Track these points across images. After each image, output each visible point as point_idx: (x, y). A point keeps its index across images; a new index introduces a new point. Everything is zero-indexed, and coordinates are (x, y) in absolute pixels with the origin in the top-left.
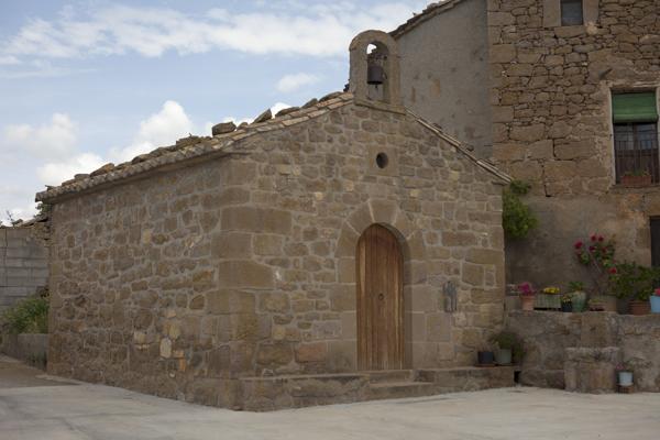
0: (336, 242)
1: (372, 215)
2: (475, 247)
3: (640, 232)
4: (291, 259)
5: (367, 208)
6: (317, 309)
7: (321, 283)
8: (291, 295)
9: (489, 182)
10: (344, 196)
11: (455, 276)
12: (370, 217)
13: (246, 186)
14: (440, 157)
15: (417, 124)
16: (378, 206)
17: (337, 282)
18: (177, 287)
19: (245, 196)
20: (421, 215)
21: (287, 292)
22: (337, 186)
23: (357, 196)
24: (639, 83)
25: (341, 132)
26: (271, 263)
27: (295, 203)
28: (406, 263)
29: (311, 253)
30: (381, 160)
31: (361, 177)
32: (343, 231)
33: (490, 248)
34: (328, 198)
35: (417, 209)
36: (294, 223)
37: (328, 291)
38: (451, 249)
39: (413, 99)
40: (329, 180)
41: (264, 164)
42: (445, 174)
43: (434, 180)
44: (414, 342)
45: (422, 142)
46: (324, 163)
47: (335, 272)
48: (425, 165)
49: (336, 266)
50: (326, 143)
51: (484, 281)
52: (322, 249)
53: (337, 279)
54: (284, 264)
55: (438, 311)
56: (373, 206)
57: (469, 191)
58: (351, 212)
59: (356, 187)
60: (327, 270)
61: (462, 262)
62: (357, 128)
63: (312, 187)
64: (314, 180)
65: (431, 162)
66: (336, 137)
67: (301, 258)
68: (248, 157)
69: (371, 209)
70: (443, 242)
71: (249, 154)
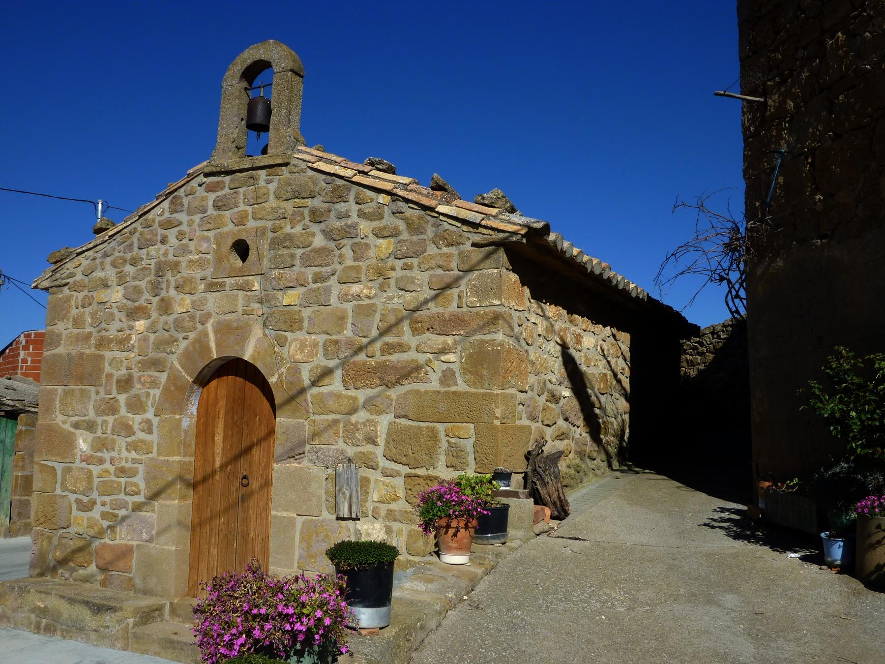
1: (213, 345)
2: (422, 387)
3: (416, 361)
4: (99, 420)
6: (126, 494)
7: (133, 454)
8: (95, 470)
9: (468, 246)
10: (176, 320)
11: (369, 448)
13: (60, 327)
14: (354, 218)
15: (310, 173)
16: (223, 329)
17: (154, 455)
18: (609, 362)
19: (56, 340)
20: (300, 335)
21: (90, 467)
22: (166, 307)
23: (192, 317)
24: (421, 586)
25: (180, 224)
26: (76, 426)
27: (110, 341)
29: (123, 411)
30: (242, 249)
31: (202, 287)
32: (169, 376)
33: (461, 386)
34: (152, 329)
36: (107, 369)
38: (362, 395)
39: (614, 336)
40: (155, 300)
41: (81, 295)
42: (359, 251)
45: (317, 203)
46: (152, 277)
47: (153, 438)
48: (319, 241)
49: (155, 430)
50: (159, 245)
51: (442, 459)
52: (136, 406)
54: (90, 427)
56: (216, 332)
57: (415, 273)
58: (183, 344)
59: (193, 302)
61: (384, 422)
62: (204, 211)
63: (134, 314)
64: (137, 304)
65: (328, 235)
66: (172, 234)
67: (110, 419)
68: (66, 288)
69: (212, 336)
70: (145, 411)
71: (67, 284)
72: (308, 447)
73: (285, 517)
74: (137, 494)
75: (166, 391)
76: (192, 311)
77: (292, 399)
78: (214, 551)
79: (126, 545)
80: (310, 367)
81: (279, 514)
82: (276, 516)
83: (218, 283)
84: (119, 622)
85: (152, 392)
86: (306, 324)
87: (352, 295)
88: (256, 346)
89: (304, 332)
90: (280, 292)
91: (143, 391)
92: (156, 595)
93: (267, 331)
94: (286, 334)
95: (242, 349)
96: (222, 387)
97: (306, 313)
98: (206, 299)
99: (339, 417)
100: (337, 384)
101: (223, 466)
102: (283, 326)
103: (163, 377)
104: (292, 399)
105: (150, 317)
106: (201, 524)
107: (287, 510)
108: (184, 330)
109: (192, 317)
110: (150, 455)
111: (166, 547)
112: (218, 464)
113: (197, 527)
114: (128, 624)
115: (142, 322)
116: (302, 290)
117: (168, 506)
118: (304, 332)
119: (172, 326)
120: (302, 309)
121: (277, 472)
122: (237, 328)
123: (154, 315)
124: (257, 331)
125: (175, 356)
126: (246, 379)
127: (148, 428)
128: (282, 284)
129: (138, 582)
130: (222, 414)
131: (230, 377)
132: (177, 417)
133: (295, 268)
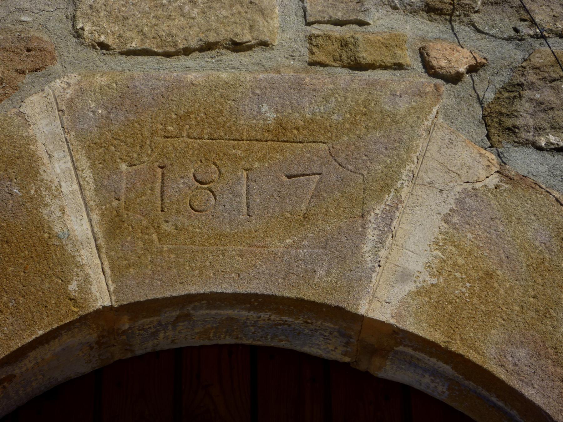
12: (44, 251)
93: (524, 161)
122: (281, 133)
124: (448, 160)
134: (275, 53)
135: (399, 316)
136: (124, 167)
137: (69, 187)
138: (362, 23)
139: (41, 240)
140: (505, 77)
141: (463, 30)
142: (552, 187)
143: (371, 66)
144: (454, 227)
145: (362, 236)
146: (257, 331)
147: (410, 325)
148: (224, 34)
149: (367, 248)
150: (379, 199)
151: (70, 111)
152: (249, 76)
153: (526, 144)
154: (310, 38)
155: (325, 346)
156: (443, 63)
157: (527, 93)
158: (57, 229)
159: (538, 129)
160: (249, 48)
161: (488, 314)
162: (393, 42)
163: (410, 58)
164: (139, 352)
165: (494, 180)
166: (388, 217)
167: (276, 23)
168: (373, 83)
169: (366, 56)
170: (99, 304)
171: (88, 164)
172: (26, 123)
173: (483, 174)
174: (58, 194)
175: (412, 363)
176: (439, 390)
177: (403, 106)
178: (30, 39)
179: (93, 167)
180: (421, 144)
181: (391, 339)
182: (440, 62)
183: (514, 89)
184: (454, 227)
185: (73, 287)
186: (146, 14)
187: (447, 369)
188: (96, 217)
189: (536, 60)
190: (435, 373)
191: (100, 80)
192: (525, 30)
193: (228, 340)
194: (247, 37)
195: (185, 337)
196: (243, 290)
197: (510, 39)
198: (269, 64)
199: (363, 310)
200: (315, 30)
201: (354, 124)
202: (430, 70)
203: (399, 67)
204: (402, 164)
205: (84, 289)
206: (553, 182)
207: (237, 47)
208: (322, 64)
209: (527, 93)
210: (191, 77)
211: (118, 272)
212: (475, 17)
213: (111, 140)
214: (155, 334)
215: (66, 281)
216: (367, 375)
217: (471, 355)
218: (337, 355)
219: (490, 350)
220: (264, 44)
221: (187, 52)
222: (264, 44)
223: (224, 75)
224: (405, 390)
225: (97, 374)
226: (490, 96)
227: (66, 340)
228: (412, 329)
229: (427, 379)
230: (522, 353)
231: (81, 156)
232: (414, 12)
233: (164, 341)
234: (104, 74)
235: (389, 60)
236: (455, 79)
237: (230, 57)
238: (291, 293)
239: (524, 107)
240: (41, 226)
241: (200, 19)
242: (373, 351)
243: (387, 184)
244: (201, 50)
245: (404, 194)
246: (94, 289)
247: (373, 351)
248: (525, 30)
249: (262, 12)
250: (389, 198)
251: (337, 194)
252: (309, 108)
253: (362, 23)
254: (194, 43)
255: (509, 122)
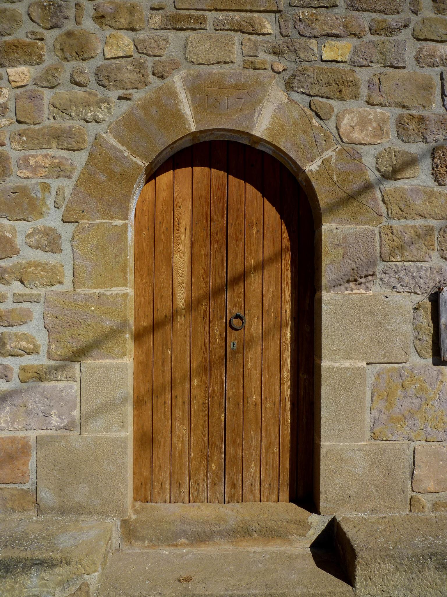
0: (67, 185)
5: (173, 94)
12: (180, 117)
16: (204, 95)
17: (68, 285)
22: (76, 48)
23: (140, 66)
28: (317, 296)
35: (343, 88)
37: (36, 310)
40: (51, 36)
43: (406, 15)
44: (322, 443)
47: (63, 260)
53: (68, 277)
55: (414, 358)
60: (38, 256)
69: (183, 96)
72: (380, 266)
73: (347, 369)
74: (34, 351)
75: (87, 180)
76: (136, 56)
77: (350, 198)
78: (182, 429)
79: (13, 440)
80: (376, 152)
81: (336, 364)
82: (332, 368)
83: (190, 16)
84: (63, 584)
85: (55, 184)
86: (364, 91)
87: (441, 57)
88: (274, 116)
89: (362, 101)
90: (314, 41)
91: (34, 181)
92: (90, 513)
93: (295, 96)
94: (330, 102)
95: (250, 118)
96: (184, 182)
97: (363, 75)
98: (167, 40)
99: (433, 223)
100: (423, 177)
101: (192, 306)
102: (325, 90)
103: (80, 159)
104: (350, 198)
105: (40, 60)
106: (154, 394)
107: (349, 358)
108: (119, 84)
109: (140, 66)
110: (58, 288)
111: (108, 435)
112: (181, 300)
113: (148, 396)
114: (86, 585)
115: (23, 69)
116: (355, 41)
117: (107, 368)
118: (362, 101)
119: (92, 78)
120: (357, 69)
121: (329, 303)
122: (236, 87)
123: (50, 59)
124: (276, 95)
125: (104, 125)
126: (229, 171)
127: (51, 242)
128: (318, 29)
129: (46, 496)
130: (185, 222)
131: (197, 169)
132: (117, 222)
133: (336, 10)
134: (235, 65)
135: (262, 135)
136: (198, 95)
137: (185, 101)
138: (257, 57)
139: (179, 114)
140: (291, 73)
141: (282, 59)
142: (300, 103)
143: (259, 69)
144: (276, 112)
145: (254, 114)
146: (229, 137)
147: (264, 137)
148: (222, 59)
149: (255, 118)
150: (259, 105)
151: (185, 80)
152: (228, 71)
153: (295, 91)
154: (244, 61)
155: (245, 141)
156: (277, 69)
157: (296, 77)
158: (183, 111)
159: (298, 87)
160: (229, 63)
161: (282, 135)
162: (264, 62)
163: (268, 67)
164: (202, 141)
165: (286, 101)
166: (261, 110)
167: (235, 56)
168: (259, 74)
169: (257, 66)
170: (193, 131)
171: (71, 516)
172: (174, 83)
173: (284, 99)
174: (182, 102)
175: (264, 146)
176: (270, 152)
177: (266, 80)
178: (174, 60)
179: (191, 95)
180: (270, 91)
181: (260, 140)
182: (276, 69)
183: (293, 76)
184: (276, 112)
185: (187, 126)
186: (203, 53)
187: (271, 147)
188: (192, 109)
189: (300, 68)
190: (269, 148)
191: (192, 72)
192: (298, 60)
193: (222, 139)
194: (228, 60)
195: (212, 138)
196: (226, 128)
197: (294, 62)
198: (233, 68)
199: (253, 134)
200: (245, 58)
201: (254, 85)
202: (273, 70)
203: (266, 69)
204: (265, 96)
205: (189, 126)
206: (300, 101)
207: (225, 63)
208: (246, 68)
209: (296, 77)
210: (214, 71)
211: (197, 123)
212: (285, 55)
213: (195, 89)
214: (205, 137)
215: (185, 125)
216: (254, 148)
217: (277, 145)
218: (247, 143)
219: (282, 144)
220: (232, 62)
221: (213, 64)
222: (232, 62)
223: (222, 71)
224: (263, 152)
225: (192, 146)
226: (287, 78)
227: (185, 139)
228: (264, 138)
229: (268, 149)
230: (289, 145)
231: (188, 92)
232: (270, 53)
233: (207, 139)
234: (193, 70)
235: (263, 67)
236: (279, 73)
237: (224, 66)
238: (237, 129)
239: (295, 81)
240: (179, 110)
241: (216, 55)
242: (256, 143)
243: (261, 101)
244: (217, 63)
245: (265, 104)
246: (192, 126)
247: (256, 143)
248: (298, 60)
249: (232, 53)
250: (261, 105)
251: (249, 104)
252: (243, 80)
253: (257, 57)
254: (215, 62)
255: (291, 85)
